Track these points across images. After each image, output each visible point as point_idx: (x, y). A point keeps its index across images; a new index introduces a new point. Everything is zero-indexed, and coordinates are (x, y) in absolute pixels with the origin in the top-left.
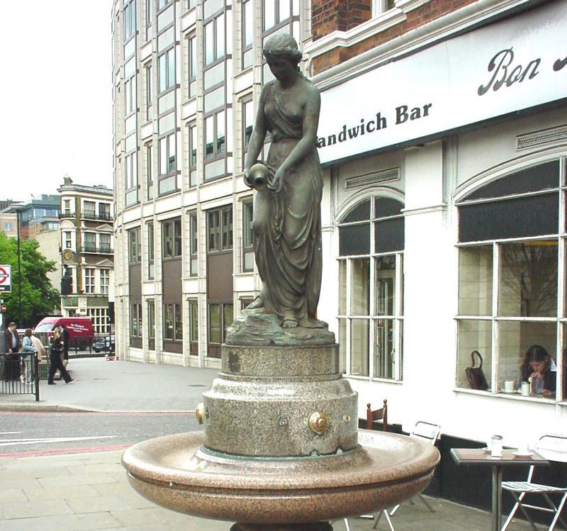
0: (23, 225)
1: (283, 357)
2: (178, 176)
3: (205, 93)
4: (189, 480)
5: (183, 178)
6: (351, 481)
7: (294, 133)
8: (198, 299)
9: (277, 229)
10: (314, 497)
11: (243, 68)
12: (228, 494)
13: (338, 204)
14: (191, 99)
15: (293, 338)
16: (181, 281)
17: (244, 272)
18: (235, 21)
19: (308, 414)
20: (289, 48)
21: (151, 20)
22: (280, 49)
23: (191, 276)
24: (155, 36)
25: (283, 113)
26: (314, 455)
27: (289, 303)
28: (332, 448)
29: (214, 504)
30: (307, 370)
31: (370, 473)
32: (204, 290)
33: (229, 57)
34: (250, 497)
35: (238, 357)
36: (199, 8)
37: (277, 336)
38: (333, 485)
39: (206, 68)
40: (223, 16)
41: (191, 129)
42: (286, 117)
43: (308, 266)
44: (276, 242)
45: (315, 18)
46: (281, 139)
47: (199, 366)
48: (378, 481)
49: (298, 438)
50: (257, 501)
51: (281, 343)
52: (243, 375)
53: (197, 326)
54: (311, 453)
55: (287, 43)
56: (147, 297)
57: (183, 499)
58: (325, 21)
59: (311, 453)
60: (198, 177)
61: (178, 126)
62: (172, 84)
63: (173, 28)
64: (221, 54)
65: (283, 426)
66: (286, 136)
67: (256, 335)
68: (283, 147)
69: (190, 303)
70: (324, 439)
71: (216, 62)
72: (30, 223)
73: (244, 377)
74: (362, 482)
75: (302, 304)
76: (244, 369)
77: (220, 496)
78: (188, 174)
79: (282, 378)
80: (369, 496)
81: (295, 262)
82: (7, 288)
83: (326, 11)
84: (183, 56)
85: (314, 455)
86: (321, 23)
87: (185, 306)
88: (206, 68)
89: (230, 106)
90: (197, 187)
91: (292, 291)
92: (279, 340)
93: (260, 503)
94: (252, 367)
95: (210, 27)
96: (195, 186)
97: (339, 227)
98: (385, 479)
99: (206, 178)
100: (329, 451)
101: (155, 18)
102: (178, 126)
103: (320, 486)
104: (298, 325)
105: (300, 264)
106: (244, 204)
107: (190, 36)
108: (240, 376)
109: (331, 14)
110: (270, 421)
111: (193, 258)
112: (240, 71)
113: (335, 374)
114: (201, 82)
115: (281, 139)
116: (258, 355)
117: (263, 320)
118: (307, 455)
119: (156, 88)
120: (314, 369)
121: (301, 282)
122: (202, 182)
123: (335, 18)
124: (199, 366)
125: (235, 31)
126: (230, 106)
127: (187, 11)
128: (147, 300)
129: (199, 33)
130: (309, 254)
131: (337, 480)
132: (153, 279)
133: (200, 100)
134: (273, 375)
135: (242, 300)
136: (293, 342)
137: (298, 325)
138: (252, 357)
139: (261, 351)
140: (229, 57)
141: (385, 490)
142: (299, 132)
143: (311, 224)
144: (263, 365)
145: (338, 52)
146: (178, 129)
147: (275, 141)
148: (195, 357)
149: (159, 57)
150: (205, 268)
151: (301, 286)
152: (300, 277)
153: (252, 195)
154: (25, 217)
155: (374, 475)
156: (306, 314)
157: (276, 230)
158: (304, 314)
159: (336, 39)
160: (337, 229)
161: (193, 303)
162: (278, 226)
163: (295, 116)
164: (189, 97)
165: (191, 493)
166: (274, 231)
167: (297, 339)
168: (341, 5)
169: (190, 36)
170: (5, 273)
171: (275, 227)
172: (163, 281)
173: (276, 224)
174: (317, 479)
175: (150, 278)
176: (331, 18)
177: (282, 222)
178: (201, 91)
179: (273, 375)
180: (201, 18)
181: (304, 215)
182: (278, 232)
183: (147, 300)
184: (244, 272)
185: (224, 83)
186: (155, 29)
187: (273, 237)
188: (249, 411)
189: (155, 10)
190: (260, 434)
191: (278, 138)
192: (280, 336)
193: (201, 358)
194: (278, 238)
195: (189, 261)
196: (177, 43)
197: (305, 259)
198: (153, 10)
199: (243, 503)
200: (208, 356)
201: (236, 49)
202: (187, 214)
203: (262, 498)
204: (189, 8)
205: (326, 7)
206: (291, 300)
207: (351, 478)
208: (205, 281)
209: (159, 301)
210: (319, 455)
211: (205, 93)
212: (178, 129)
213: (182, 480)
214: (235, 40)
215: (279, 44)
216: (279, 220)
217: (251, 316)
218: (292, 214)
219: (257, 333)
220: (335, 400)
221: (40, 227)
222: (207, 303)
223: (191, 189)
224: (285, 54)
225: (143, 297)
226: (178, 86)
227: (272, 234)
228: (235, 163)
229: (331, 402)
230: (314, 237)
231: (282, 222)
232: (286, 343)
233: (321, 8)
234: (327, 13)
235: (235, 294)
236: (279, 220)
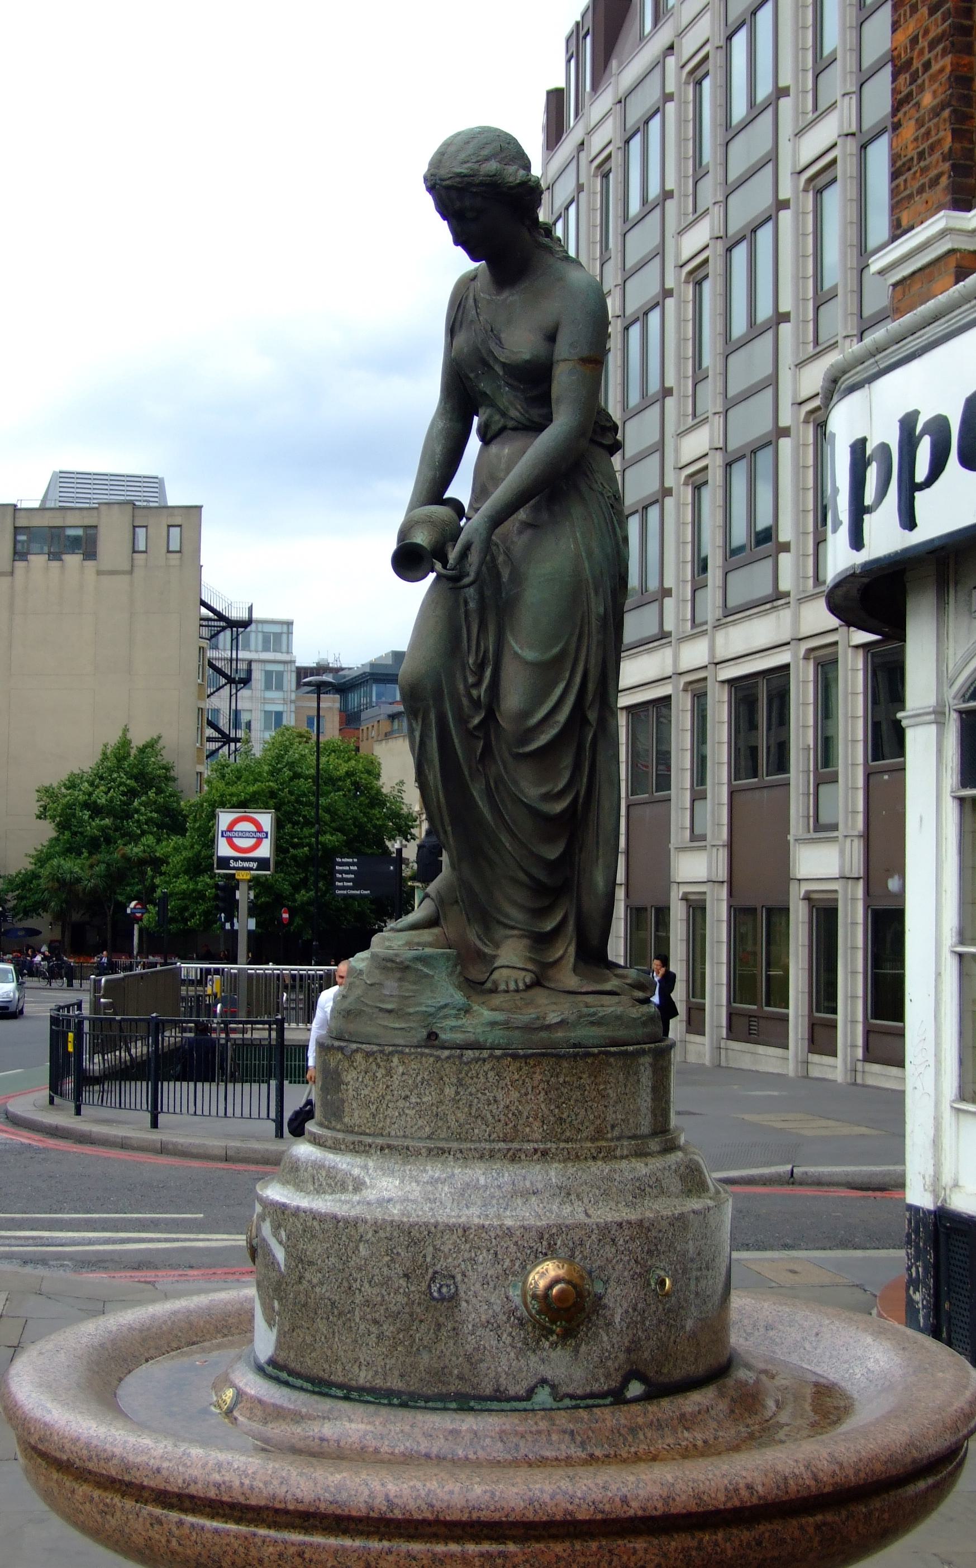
0: (350, 719)
1: (460, 1083)
2: (666, 600)
3: (730, 404)
4: (108, 1460)
5: (678, 607)
6: (566, 1510)
7: (535, 413)
8: (840, 897)
9: (474, 692)
10: (471, 1548)
11: (816, 342)
12: (212, 1517)
13: (955, 653)
14: (699, 420)
15: (493, 1024)
16: (788, 842)
17: (815, 831)
18: (799, 234)
19: (524, 1268)
20: (492, 166)
21: (611, 245)
22: (463, 169)
23: (691, 841)
24: (620, 281)
25: (496, 359)
26: (543, 1396)
27: (516, 915)
28: (608, 1376)
29: (174, 1543)
30: (536, 1124)
31: (669, 1478)
32: (723, 874)
33: (784, 318)
34: (272, 1533)
35: (339, 1075)
36: (717, 211)
37: (446, 1017)
38: (530, 1516)
39: (731, 347)
40: (769, 227)
41: (697, 488)
42: (504, 365)
43: (575, 800)
44: (470, 735)
45: (898, 186)
46: (503, 429)
47: (707, 1061)
48: (694, 1508)
49: (489, 1340)
50: (292, 1550)
51: (458, 1037)
52: (349, 1130)
53: (704, 963)
54: (531, 1392)
55: (485, 152)
56: (805, 887)
57: (98, 1518)
58: (921, 190)
59: (531, 1392)
60: (711, 600)
61: (667, 485)
62: (654, 386)
63: (657, 260)
64: (764, 311)
65: (443, 1299)
66: (511, 424)
67: (390, 1011)
68: (504, 450)
69: (689, 907)
70: (578, 1346)
71: (755, 330)
72: (363, 716)
73: (350, 1138)
74: (635, 1508)
75: (558, 918)
76: (355, 1115)
77: (190, 1519)
78: (689, 596)
79: (455, 1145)
80: (665, 1555)
81: (531, 791)
82: (263, 863)
83: (922, 164)
84: (680, 321)
85: (543, 1396)
86: (910, 196)
87: (678, 913)
88: (731, 347)
89: (785, 432)
90: (708, 627)
91: (522, 876)
92: (452, 1029)
93: (301, 1555)
94: (373, 1108)
95: (740, 254)
96: (706, 623)
97: (960, 712)
98: (720, 1501)
99: (730, 604)
100: (596, 1387)
101: (620, 238)
102: (667, 485)
103: (485, 1515)
104: (537, 983)
105: (548, 797)
106: (817, 665)
107: (697, 277)
108: (340, 1136)
109: (933, 173)
110: (403, 1282)
111: (698, 796)
112: (810, 349)
113: (654, 1134)
114: (720, 380)
115: (503, 429)
116: (389, 1073)
117: (407, 967)
118: (518, 1399)
119: (619, 398)
120: (561, 1120)
121: (553, 852)
122: (719, 613)
123: (944, 181)
124: (707, 1061)
125: (799, 257)
126: (785, 432)
127: (691, 218)
128: (685, 898)
129: (715, 268)
130: (577, 767)
131: (546, 1497)
132: (703, 838)
133: (718, 421)
134: (429, 1138)
135: (687, 900)
136: (496, 1036)
137: (537, 983)
138: (374, 1078)
139: (395, 1060)
140: (784, 318)
141: (699, 1548)
142: (544, 411)
143: (578, 680)
144: (401, 1103)
145: (952, 262)
146: (667, 492)
147: (486, 439)
148: (697, 1039)
149: (626, 329)
150: (725, 819)
151: (552, 866)
152: (550, 839)
153: (836, 643)
154: (355, 699)
155: (680, 1486)
156: (572, 950)
157: (469, 695)
158: (566, 950)
159: (943, 233)
160: (954, 716)
161: (697, 909)
162: (477, 684)
163: (527, 362)
164: (694, 415)
165: (117, 1500)
166: (465, 701)
167: (507, 1025)
168: (958, 146)
169: (697, 277)
170: (259, 828)
171: (468, 688)
172: (731, 845)
173: (471, 680)
174: (478, 1490)
175: (693, 838)
176: (934, 182)
177: (488, 673)
178: (720, 400)
179: (429, 1138)
180: (721, 234)
181: (556, 650)
182: (476, 704)
183: (685, 898)
184: (815, 831)
185: (773, 381)
186: (620, 265)
187: (462, 720)
188: (346, 1247)
189: (620, 221)
190: (376, 1322)
191: (495, 428)
192: (457, 1017)
193: (712, 1039)
194: (476, 721)
195: (688, 805)
196: (667, 293)
197: (561, 785)
198: (616, 222)
199: (253, 1552)
200: (728, 1038)
201: (800, 300)
202: (685, 690)
203: (307, 1538)
204: (695, 211)
205: (921, 156)
206: (521, 907)
207: (597, 1495)
208: (723, 854)
209: (719, 900)
210: (561, 1400)
211: (730, 404)
212: (667, 492)
213: (90, 1459)
214: (799, 278)
215: (462, 156)
216: (481, 666)
217: (377, 956)
218: (517, 649)
219: (389, 1006)
220: (620, 1225)
221: (385, 726)
222: (730, 907)
223: (695, 631)
224: (481, 184)
225: (674, 887)
226: (667, 392)
227: (458, 708)
228: (797, 566)
229: (604, 1230)
230: (592, 716)
231: (488, 673)
232: (471, 1037)
233: (912, 159)
234: (924, 170)
235: (793, 887)
236: (481, 666)
